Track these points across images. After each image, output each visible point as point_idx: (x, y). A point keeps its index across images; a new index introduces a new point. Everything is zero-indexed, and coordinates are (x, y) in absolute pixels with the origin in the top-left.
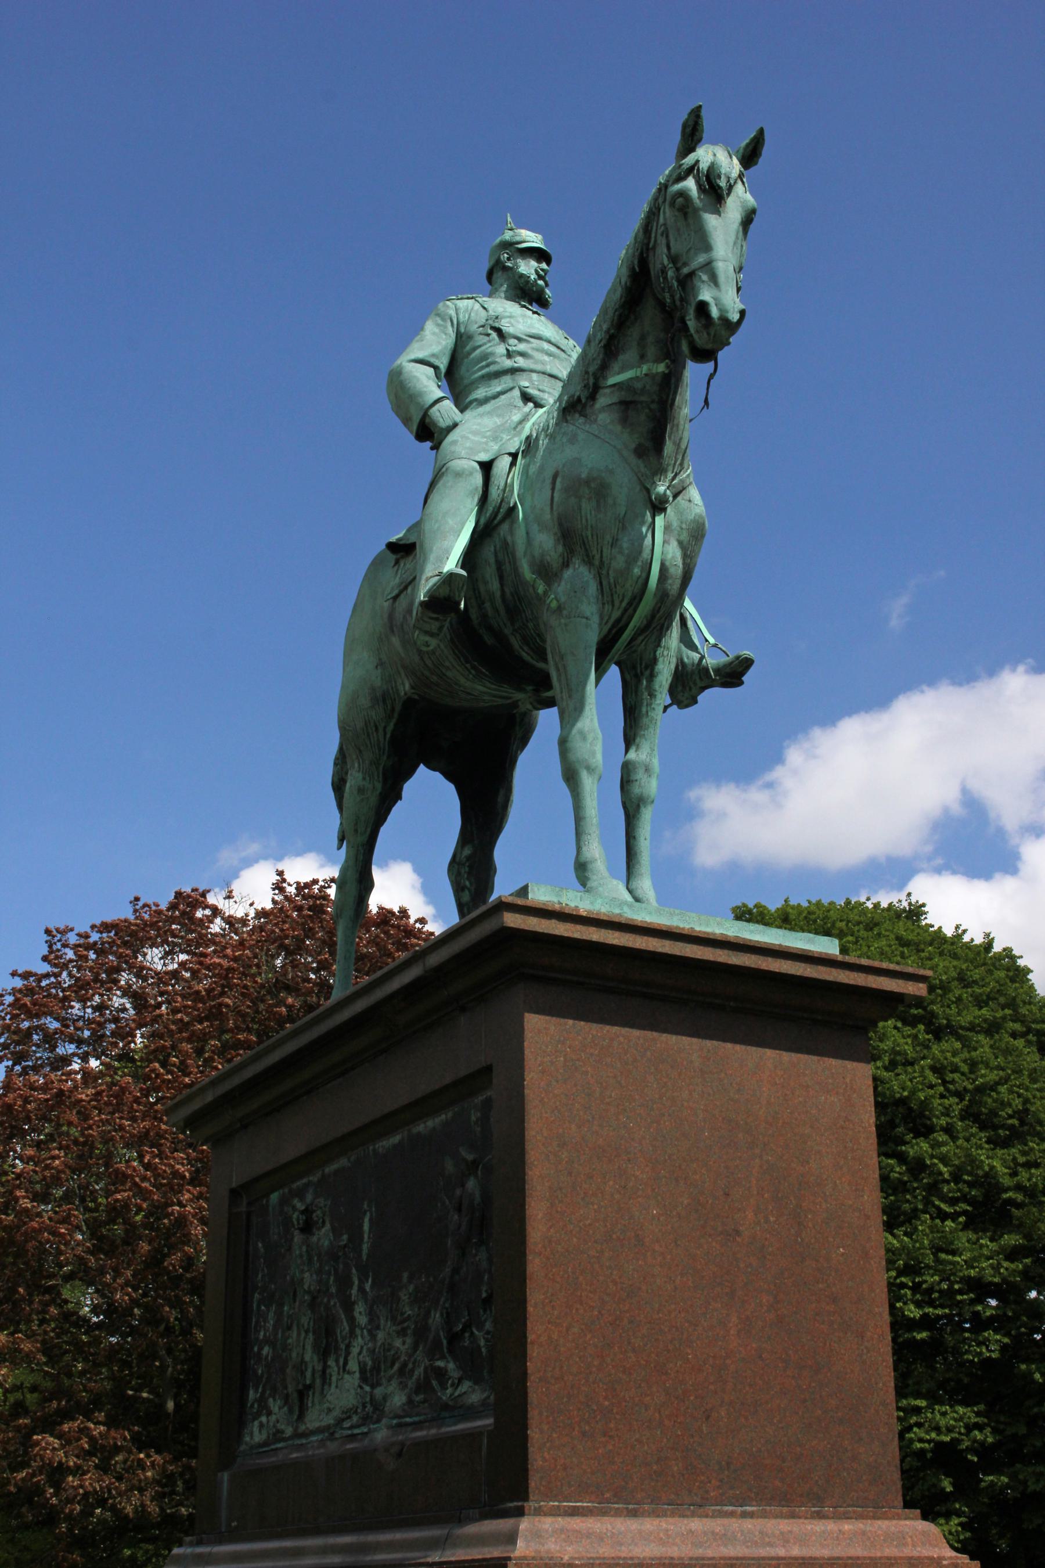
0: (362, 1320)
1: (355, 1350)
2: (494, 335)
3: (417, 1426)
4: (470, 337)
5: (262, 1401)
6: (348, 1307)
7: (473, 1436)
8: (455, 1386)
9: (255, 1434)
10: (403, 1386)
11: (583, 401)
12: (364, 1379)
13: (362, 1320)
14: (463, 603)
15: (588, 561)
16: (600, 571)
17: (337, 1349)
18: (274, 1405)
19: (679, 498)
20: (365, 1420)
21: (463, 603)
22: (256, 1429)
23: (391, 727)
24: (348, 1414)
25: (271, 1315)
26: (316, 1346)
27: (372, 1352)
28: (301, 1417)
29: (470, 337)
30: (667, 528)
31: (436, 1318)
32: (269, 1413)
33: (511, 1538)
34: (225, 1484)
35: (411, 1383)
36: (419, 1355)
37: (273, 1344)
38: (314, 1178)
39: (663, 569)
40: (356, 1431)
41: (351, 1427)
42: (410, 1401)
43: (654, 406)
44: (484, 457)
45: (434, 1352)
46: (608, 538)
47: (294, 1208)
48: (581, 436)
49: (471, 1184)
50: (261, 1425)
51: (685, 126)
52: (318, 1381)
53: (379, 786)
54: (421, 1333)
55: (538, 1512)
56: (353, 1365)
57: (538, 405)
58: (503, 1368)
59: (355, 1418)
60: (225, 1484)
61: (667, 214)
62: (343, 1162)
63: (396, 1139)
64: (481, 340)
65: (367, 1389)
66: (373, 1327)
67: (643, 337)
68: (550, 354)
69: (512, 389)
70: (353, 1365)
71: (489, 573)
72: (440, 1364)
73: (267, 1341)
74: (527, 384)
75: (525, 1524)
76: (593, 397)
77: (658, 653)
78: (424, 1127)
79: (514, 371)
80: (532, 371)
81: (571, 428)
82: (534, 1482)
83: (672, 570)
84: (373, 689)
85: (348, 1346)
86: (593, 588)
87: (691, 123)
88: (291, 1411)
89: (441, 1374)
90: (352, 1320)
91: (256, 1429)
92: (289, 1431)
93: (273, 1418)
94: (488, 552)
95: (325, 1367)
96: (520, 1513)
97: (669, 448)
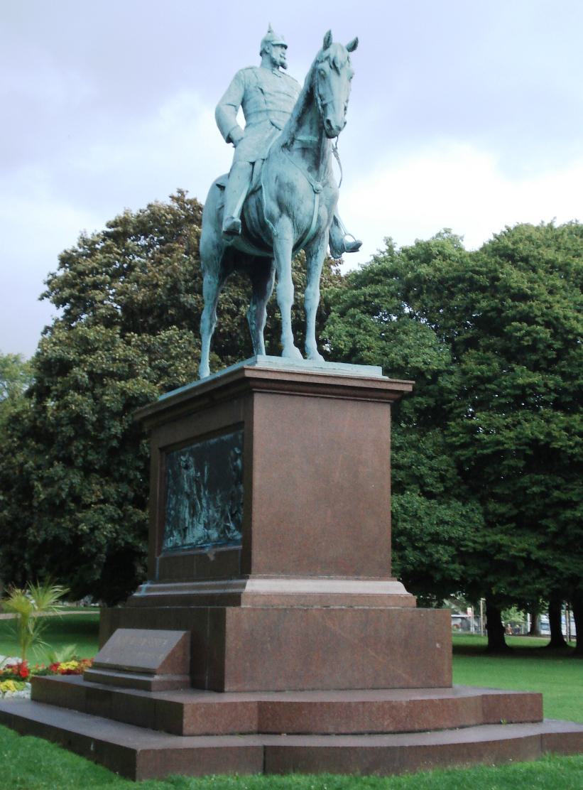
0: (205, 505)
1: (202, 516)
2: (259, 91)
3: (221, 546)
4: (250, 92)
5: (171, 531)
6: (200, 500)
7: (236, 551)
8: (233, 532)
9: (169, 544)
10: (217, 530)
11: (289, 144)
12: (205, 527)
13: (205, 505)
14: (92, 746)
15: (289, 215)
17: (197, 515)
18: (175, 533)
19: (326, 187)
20: (205, 542)
21: (92, 746)
22: (169, 542)
23: (221, 257)
24: (200, 538)
25: (174, 499)
26: (189, 513)
27: (208, 517)
28: (185, 536)
29: (250, 92)
30: (320, 200)
31: (227, 508)
32: (173, 536)
33: (244, 586)
34: (207, 681)
35: (220, 530)
36: (222, 520)
37: (175, 510)
38: (189, 449)
39: (319, 219)
40: (203, 546)
41: (201, 544)
42: (219, 536)
43: (315, 150)
44: (252, 160)
45: (226, 520)
46: (296, 208)
47: (181, 460)
48: (287, 161)
49: (239, 462)
50: (171, 541)
51: (325, 39)
52: (191, 526)
53: (217, 281)
54: (223, 513)
55: (254, 578)
56: (202, 521)
57: (280, 130)
58: (245, 526)
59: (202, 541)
60: (207, 681)
61: (317, 76)
62: (198, 445)
63: (215, 440)
64: (254, 94)
65: (206, 530)
66: (208, 508)
67: (311, 120)
68: (284, 100)
69: (266, 120)
70: (202, 521)
71: (253, 210)
72: (228, 524)
73: (173, 509)
74: (273, 117)
75: (249, 582)
76: (292, 143)
78: (226, 437)
79: (268, 111)
80: (275, 110)
81: (284, 155)
82: (253, 568)
83: (322, 217)
84: (213, 242)
85: (200, 514)
87: (327, 38)
88: (181, 536)
89: (228, 528)
90: (201, 504)
91: (169, 542)
92: (180, 543)
93: (175, 538)
94: (253, 201)
95: (193, 521)
96: (248, 578)
97: (322, 167)
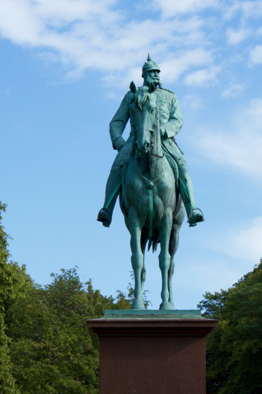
15: (134, 206)
16: (137, 208)
43: (145, 159)
77: (163, 224)
86: (136, 214)
